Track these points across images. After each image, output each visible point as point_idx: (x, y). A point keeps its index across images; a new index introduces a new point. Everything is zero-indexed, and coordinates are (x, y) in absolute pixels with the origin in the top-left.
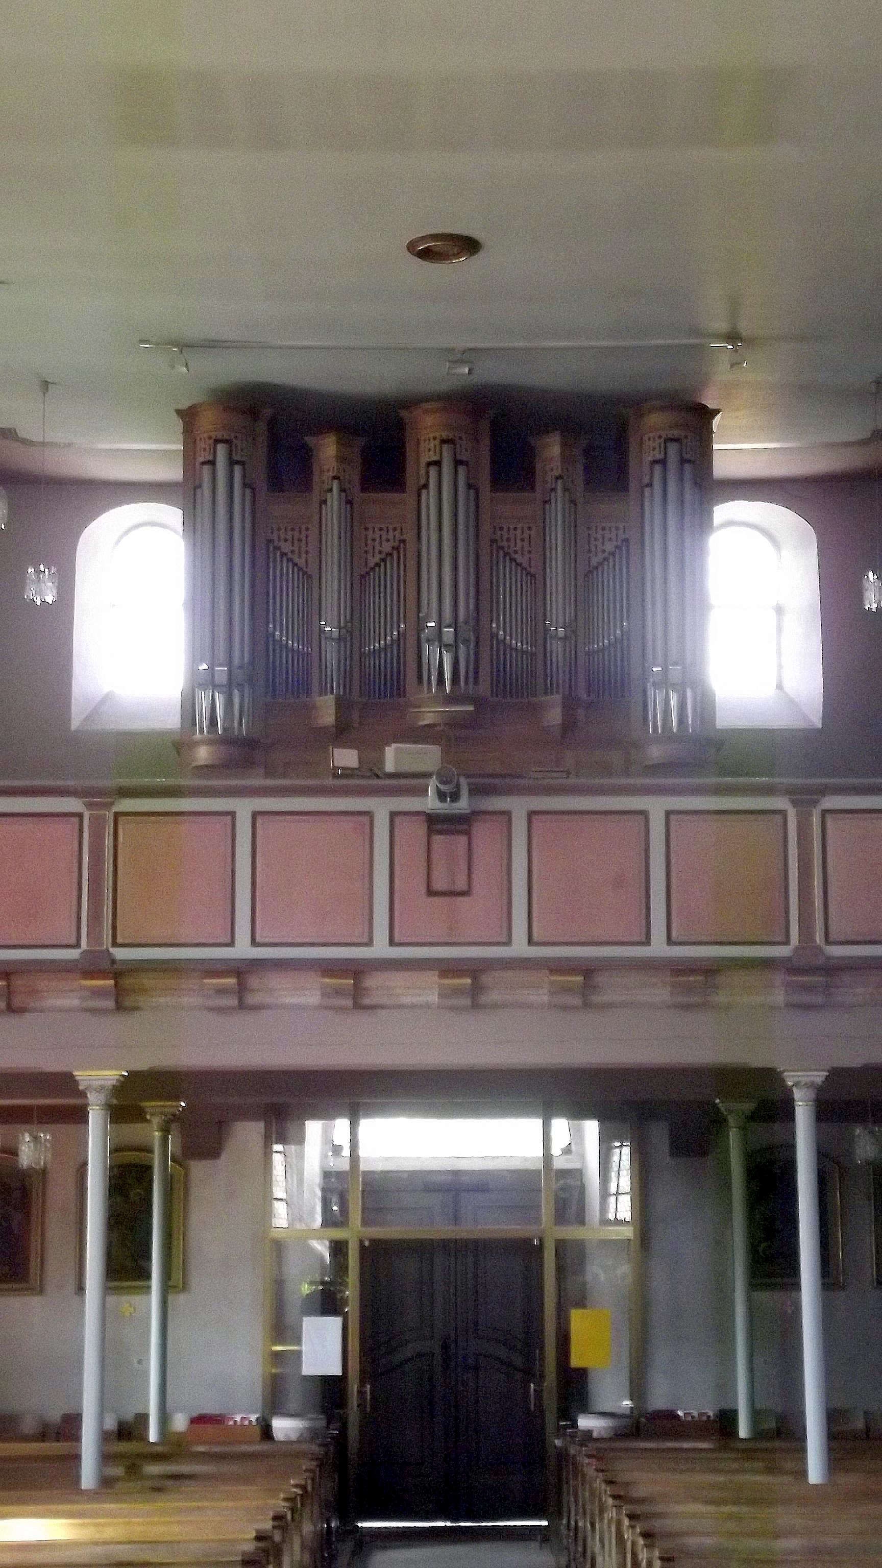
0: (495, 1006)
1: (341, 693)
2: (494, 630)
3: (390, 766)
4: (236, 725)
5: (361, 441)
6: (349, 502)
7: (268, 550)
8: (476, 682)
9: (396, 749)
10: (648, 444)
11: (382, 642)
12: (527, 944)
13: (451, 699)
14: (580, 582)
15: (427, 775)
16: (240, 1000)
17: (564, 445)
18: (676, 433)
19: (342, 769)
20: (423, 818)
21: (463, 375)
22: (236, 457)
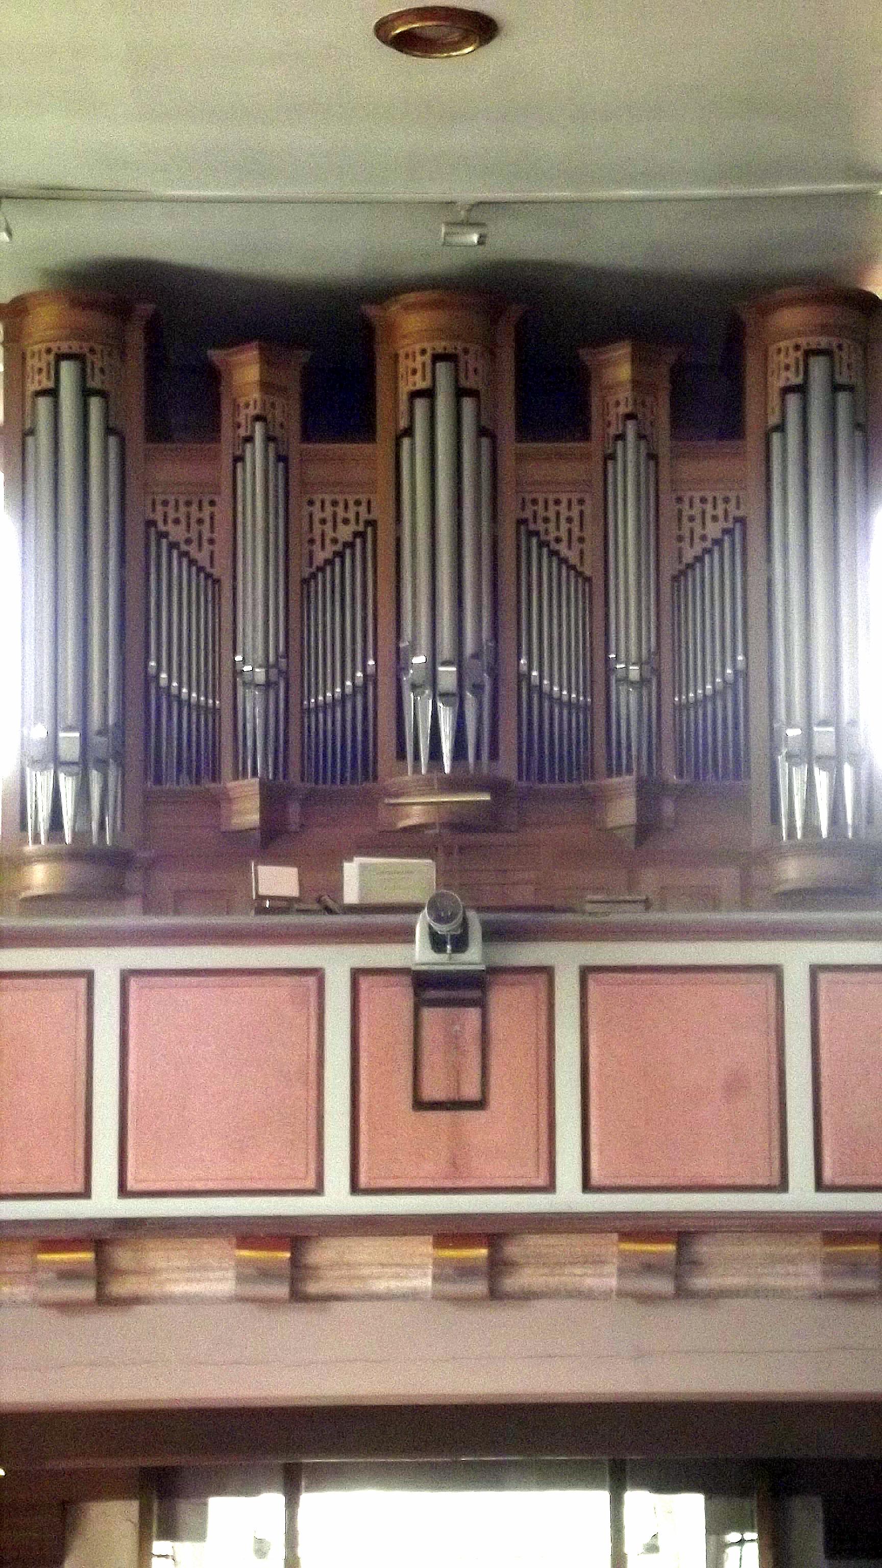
0: (527, 1296)
1: (271, 777)
2: (524, 669)
3: (351, 895)
4: (95, 826)
5: (304, 356)
6: (282, 458)
7: (147, 538)
8: (494, 755)
9: (363, 867)
10: (404, 365)
11: (709, 687)
12: (813, 1190)
13: (453, 784)
14: (666, 589)
15: (416, 909)
16: (100, 1285)
17: (637, 360)
18: (823, 342)
19: (271, 898)
20: (407, 980)
21: (472, 246)
22: (841, 379)
